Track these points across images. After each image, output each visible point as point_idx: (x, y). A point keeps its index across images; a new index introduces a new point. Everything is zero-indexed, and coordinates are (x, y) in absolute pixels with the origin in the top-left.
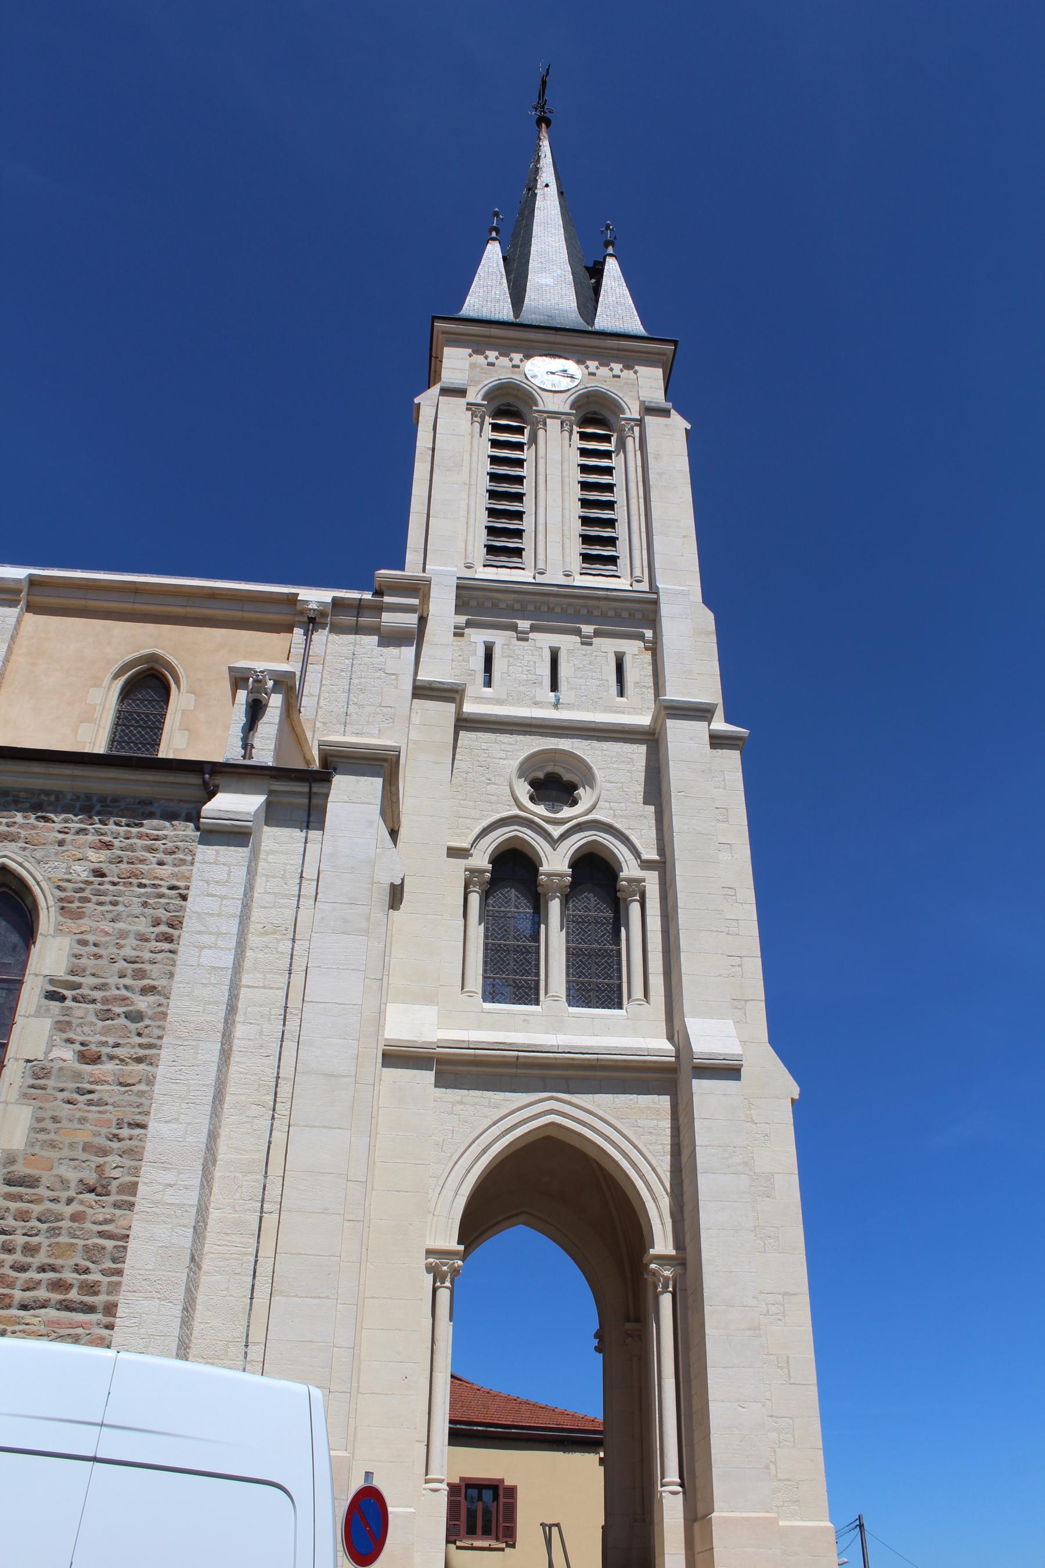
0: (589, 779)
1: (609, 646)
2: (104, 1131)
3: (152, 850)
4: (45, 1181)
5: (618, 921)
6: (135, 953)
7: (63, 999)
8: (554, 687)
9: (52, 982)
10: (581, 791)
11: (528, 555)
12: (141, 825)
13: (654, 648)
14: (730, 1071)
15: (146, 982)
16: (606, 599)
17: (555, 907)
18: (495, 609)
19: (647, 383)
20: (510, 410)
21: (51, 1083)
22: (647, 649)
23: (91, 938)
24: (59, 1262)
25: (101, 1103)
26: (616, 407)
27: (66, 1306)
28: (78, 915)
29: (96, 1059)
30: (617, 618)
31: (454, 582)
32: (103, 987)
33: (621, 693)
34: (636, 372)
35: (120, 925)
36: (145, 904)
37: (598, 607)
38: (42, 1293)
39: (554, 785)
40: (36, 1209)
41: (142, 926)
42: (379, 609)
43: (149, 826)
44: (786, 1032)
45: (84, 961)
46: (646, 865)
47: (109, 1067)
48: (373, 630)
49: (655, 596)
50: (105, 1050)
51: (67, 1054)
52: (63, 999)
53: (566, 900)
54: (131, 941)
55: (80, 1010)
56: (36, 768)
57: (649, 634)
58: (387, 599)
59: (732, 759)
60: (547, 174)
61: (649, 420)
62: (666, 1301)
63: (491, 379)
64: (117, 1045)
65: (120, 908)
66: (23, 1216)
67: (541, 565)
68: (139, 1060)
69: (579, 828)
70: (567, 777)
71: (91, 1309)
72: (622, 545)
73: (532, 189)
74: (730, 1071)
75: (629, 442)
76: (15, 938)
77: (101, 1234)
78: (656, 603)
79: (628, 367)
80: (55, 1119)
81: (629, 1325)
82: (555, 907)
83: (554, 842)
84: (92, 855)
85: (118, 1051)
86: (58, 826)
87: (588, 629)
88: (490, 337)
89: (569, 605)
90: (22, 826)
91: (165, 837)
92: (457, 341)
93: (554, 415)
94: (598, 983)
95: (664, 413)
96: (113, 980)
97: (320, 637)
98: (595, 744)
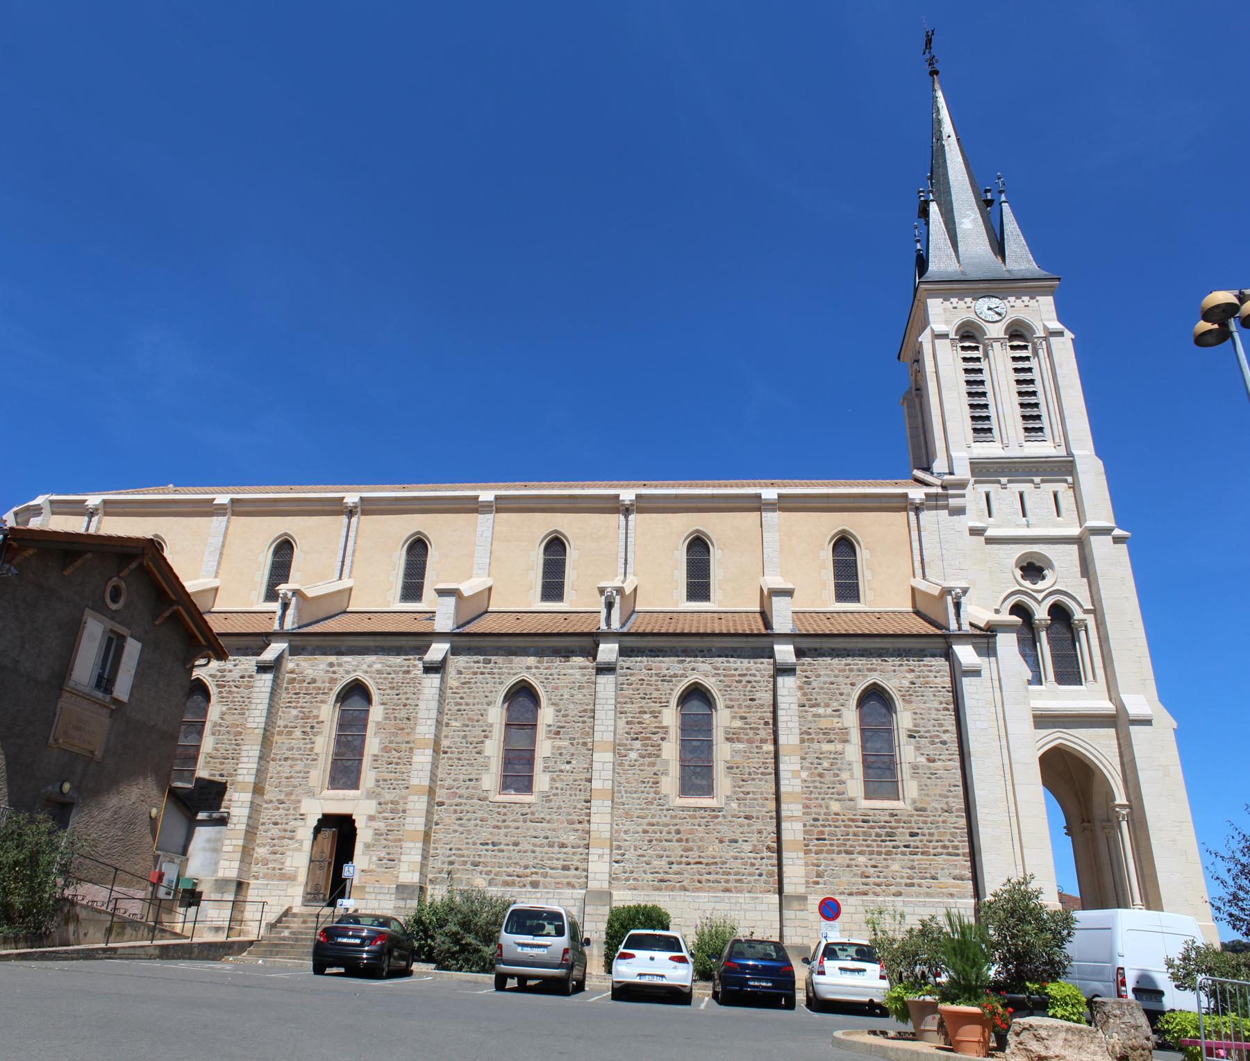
0: (1050, 566)
1: (1049, 488)
5: (1074, 640)
11: (996, 431)
13: (1074, 487)
14: (1147, 722)
17: (1043, 635)
18: (988, 473)
19: (1041, 312)
20: (969, 334)
28: (911, 702)
29: (934, 761)
30: (1052, 473)
31: (968, 462)
33: (1058, 515)
38: (939, 850)
39: (1032, 569)
40: (929, 819)
42: (947, 497)
43: (927, 660)
46: (1086, 611)
47: (939, 763)
48: (946, 507)
51: (923, 760)
53: (1048, 628)
54: (934, 712)
57: (1070, 479)
58: (950, 492)
59: (1124, 547)
61: (1052, 339)
62: (1124, 824)
63: (957, 322)
67: (1005, 441)
69: (1050, 594)
70: (1038, 564)
72: (1045, 418)
73: (940, 139)
74: (1147, 722)
75: (1040, 352)
76: (884, 711)
78: (1073, 462)
79: (1032, 298)
81: (1085, 824)
82: (1043, 635)
83: (1039, 603)
87: (1037, 480)
92: (934, 294)
93: (997, 340)
94: (1069, 673)
95: (1061, 334)
97: (924, 515)
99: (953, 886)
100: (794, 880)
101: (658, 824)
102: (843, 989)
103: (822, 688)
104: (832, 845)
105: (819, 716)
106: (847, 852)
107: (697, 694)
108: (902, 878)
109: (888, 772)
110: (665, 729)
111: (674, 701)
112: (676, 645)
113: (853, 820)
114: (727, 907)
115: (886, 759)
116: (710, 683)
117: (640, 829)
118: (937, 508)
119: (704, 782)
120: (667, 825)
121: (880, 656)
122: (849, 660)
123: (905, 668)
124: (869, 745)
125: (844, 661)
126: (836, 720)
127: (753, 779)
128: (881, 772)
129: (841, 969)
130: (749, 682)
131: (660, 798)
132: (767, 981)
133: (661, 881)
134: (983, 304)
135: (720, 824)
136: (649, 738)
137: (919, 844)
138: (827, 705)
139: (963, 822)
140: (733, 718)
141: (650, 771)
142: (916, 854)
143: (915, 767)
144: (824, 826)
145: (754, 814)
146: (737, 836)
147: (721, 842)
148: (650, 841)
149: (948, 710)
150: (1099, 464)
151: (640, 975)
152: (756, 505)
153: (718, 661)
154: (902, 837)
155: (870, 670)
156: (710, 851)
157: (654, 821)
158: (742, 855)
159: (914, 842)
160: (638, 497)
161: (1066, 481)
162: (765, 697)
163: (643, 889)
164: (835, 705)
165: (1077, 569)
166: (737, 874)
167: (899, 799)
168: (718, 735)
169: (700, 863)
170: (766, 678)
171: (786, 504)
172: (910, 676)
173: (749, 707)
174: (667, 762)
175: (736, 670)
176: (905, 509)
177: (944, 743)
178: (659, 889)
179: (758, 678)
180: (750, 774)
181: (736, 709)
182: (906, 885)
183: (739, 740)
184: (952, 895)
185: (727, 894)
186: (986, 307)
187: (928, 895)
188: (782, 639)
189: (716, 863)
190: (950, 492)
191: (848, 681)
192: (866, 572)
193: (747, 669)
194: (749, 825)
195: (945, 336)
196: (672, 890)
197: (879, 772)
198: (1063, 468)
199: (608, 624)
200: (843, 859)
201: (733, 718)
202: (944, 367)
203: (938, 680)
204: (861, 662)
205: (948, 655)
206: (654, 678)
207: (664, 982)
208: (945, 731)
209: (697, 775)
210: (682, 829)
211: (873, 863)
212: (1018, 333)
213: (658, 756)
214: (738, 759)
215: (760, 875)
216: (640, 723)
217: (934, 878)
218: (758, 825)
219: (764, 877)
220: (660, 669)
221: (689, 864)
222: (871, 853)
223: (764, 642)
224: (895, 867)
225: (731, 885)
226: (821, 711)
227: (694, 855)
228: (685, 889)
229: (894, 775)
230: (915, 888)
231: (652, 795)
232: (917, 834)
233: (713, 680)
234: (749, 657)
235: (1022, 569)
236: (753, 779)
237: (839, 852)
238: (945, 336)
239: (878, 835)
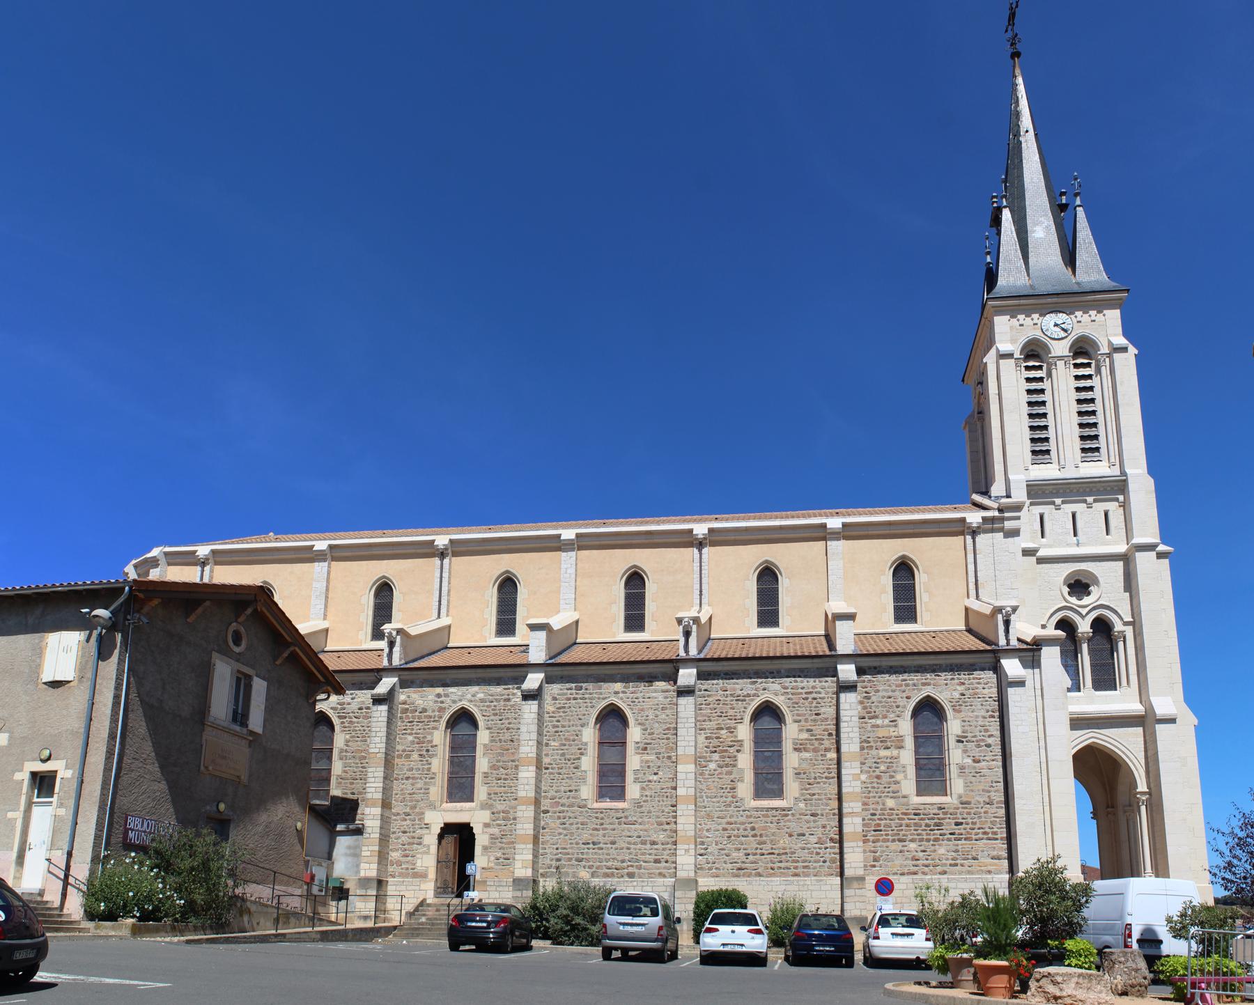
0: (1096, 581)
1: (1100, 507)
5: (1113, 649)
8: (1075, 535)
10: (1091, 588)
11: (1054, 453)
13: (1125, 506)
14: (1172, 721)
17: (1085, 647)
19: (1107, 327)
26: (1094, 344)
27: (989, 839)
29: (979, 761)
39: (1079, 586)
41: (983, 713)
42: (1003, 519)
43: (977, 674)
44: (1191, 698)
46: (1126, 624)
47: (983, 763)
48: (1001, 530)
51: (969, 761)
53: (1089, 640)
56: (932, 657)
57: (1121, 498)
58: (1006, 515)
60: (1026, 122)
62: (1143, 808)
63: (1023, 340)
66: (969, 813)
67: (1062, 463)
69: (1094, 608)
74: (1172, 721)
76: (936, 719)
78: (1125, 481)
82: (1085, 647)
83: (1083, 617)
84: (959, 688)
87: (1090, 499)
92: (1001, 311)
93: (1060, 358)
94: (1105, 679)
97: (980, 538)
98: (1098, 564)
100: (853, 865)
105: (878, 726)
106: (900, 840)
107: (768, 711)
111: (747, 718)
115: (937, 762)
116: (779, 701)
117: (720, 827)
118: (992, 531)
119: (775, 787)
120: (743, 823)
121: (934, 671)
122: (906, 676)
124: (921, 750)
125: (901, 677)
128: (931, 772)
131: (737, 802)
135: (789, 821)
138: (885, 717)
139: (1002, 812)
140: (801, 730)
143: (962, 768)
146: (804, 830)
147: (791, 835)
150: (1150, 483)
152: (821, 534)
153: (787, 681)
154: (948, 826)
155: (924, 684)
157: (733, 820)
159: (957, 830)
160: (711, 530)
161: (1117, 500)
164: (892, 716)
165: (1120, 584)
166: (804, 861)
168: (787, 746)
172: (961, 688)
173: (815, 720)
174: (742, 770)
176: (962, 533)
177: (988, 746)
181: (803, 723)
183: (806, 750)
184: (990, 872)
187: (969, 872)
188: (844, 660)
191: (904, 695)
193: (813, 687)
195: (1010, 356)
198: (1116, 488)
199: (687, 651)
200: (897, 846)
201: (801, 730)
202: (1007, 386)
203: (986, 691)
205: (996, 668)
207: (744, 949)
208: (990, 736)
209: (769, 780)
212: (1083, 350)
213: (734, 766)
214: (804, 766)
217: (974, 859)
222: (921, 840)
224: (942, 851)
225: (800, 870)
226: (879, 722)
227: (767, 848)
228: (760, 875)
229: (943, 775)
230: (959, 868)
231: (730, 799)
233: (782, 698)
234: (815, 677)
235: (1070, 586)
237: (894, 841)
239: (927, 825)
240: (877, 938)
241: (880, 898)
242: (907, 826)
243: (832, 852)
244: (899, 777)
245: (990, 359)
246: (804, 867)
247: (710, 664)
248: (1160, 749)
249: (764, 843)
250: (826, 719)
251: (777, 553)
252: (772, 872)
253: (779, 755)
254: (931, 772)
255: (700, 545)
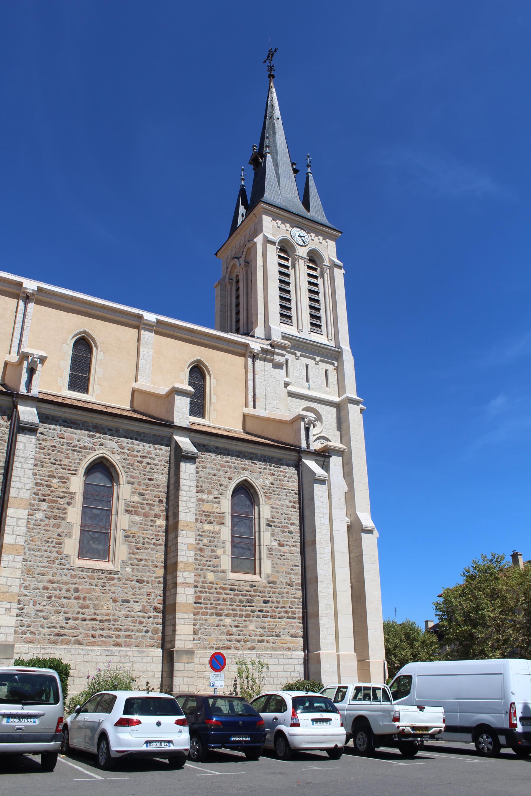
1: (324, 366)
2: (289, 568)
3: (285, 476)
4: (278, 583)
6: (287, 512)
7: (271, 526)
9: (268, 520)
12: (280, 467)
15: (291, 521)
16: (325, 348)
19: (328, 250)
20: (285, 248)
21: (273, 553)
22: (335, 369)
23: (275, 506)
24: (285, 606)
25: (287, 559)
27: (289, 618)
28: (270, 498)
32: (280, 523)
34: (327, 242)
35: (281, 502)
36: (286, 495)
37: (322, 351)
40: (277, 591)
41: (287, 503)
42: (273, 353)
45: (274, 514)
47: (286, 548)
48: (271, 361)
49: (340, 350)
50: (285, 543)
51: (276, 544)
52: (271, 526)
54: (285, 508)
55: (277, 530)
56: (252, 446)
57: (336, 363)
58: (277, 350)
64: (288, 541)
65: (280, 496)
67: (300, 327)
68: (294, 546)
71: (295, 618)
75: (325, 275)
76: (248, 503)
77: (294, 598)
80: (277, 564)
85: (288, 543)
86: (258, 466)
87: (318, 359)
88: (279, 214)
89: (313, 348)
90: (248, 465)
91: (288, 472)
92: (269, 213)
93: (302, 258)
96: (283, 520)
99: (290, 642)
100: (184, 637)
101: (58, 582)
102: (316, 738)
103: (207, 478)
104: (206, 608)
105: (203, 500)
106: (218, 615)
107: (102, 468)
108: (256, 635)
109: (248, 552)
110: (72, 495)
111: (82, 471)
112: (89, 420)
113: (223, 589)
114: (117, 659)
115: (248, 541)
116: (115, 459)
117: (40, 585)
118: (265, 360)
119: (101, 547)
120: (66, 583)
121: (251, 459)
122: (229, 458)
123: (268, 471)
124: (236, 529)
125: (225, 459)
126: (216, 505)
127: (146, 548)
128: (245, 551)
129: (313, 720)
130: (149, 464)
131: (61, 558)
132: (245, 735)
133: (57, 635)
134: (296, 232)
135: (115, 585)
136: (56, 502)
137: (269, 609)
138: (210, 493)
139: (299, 593)
140: (133, 493)
141: (53, 532)
142: (266, 617)
143: (270, 550)
144: (201, 592)
145: (145, 579)
146: (130, 597)
147: (115, 601)
148: (50, 597)
149: (294, 507)
151: (147, 742)
152: (137, 323)
153: (124, 441)
154: (258, 604)
155: (243, 469)
156: (104, 609)
157: (55, 578)
158: (133, 613)
159: (267, 607)
160: (40, 289)
161: (333, 364)
162: (162, 479)
163: (39, 642)
164: (216, 493)
166: (127, 630)
167: (255, 574)
168: (119, 507)
169: (95, 619)
170: (163, 463)
171: (160, 329)
172: (271, 478)
173: (147, 485)
174: (71, 525)
175: (138, 451)
177: (291, 532)
178: (55, 643)
179: (156, 462)
180: (144, 543)
181: (136, 486)
182: (259, 641)
183: (137, 513)
184: (289, 649)
185: (117, 648)
186: (297, 234)
187: (273, 649)
188: (180, 432)
189: (109, 620)
190: (277, 350)
191: (227, 475)
192: (213, 397)
193: (148, 452)
194: (140, 588)
195: (273, 243)
196: (67, 644)
197: (242, 551)
198: (333, 355)
199: (28, 388)
200: (214, 620)
201: (133, 493)
203: (290, 484)
204: (237, 462)
205: (298, 465)
206: (65, 447)
207: (172, 747)
208: (292, 524)
209: (96, 539)
210: (80, 588)
211: (236, 623)
212: (314, 258)
213: (63, 519)
214: (135, 529)
215: (147, 632)
216: (48, 486)
217: (278, 636)
218: (147, 589)
219: (150, 634)
220: (71, 439)
221: (84, 620)
222: (235, 615)
223: (165, 431)
224: (252, 627)
225: (122, 640)
226: (205, 496)
227: (90, 612)
228: (79, 643)
229: (253, 554)
230: (265, 644)
231: (54, 555)
232: (268, 602)
233: (118, 457)
234: (150, 442)
236: (146, 548)
237: (212, 614)
238: (273, 243)
239: (241, 601)
240: (298, 725)
241: (213, 674)
242: (224, 600)
243: (155, 621)
244: (219, 552)
245: (259, 240)
246: (127, 637)
247: (51, 407)
248: (364, 553)
249: (88, 607)
250: (158, 485)
251: (97, 329)
252: (93, 639)
253: (108, 514)
254: (245, 551)
255: (27, 298)
